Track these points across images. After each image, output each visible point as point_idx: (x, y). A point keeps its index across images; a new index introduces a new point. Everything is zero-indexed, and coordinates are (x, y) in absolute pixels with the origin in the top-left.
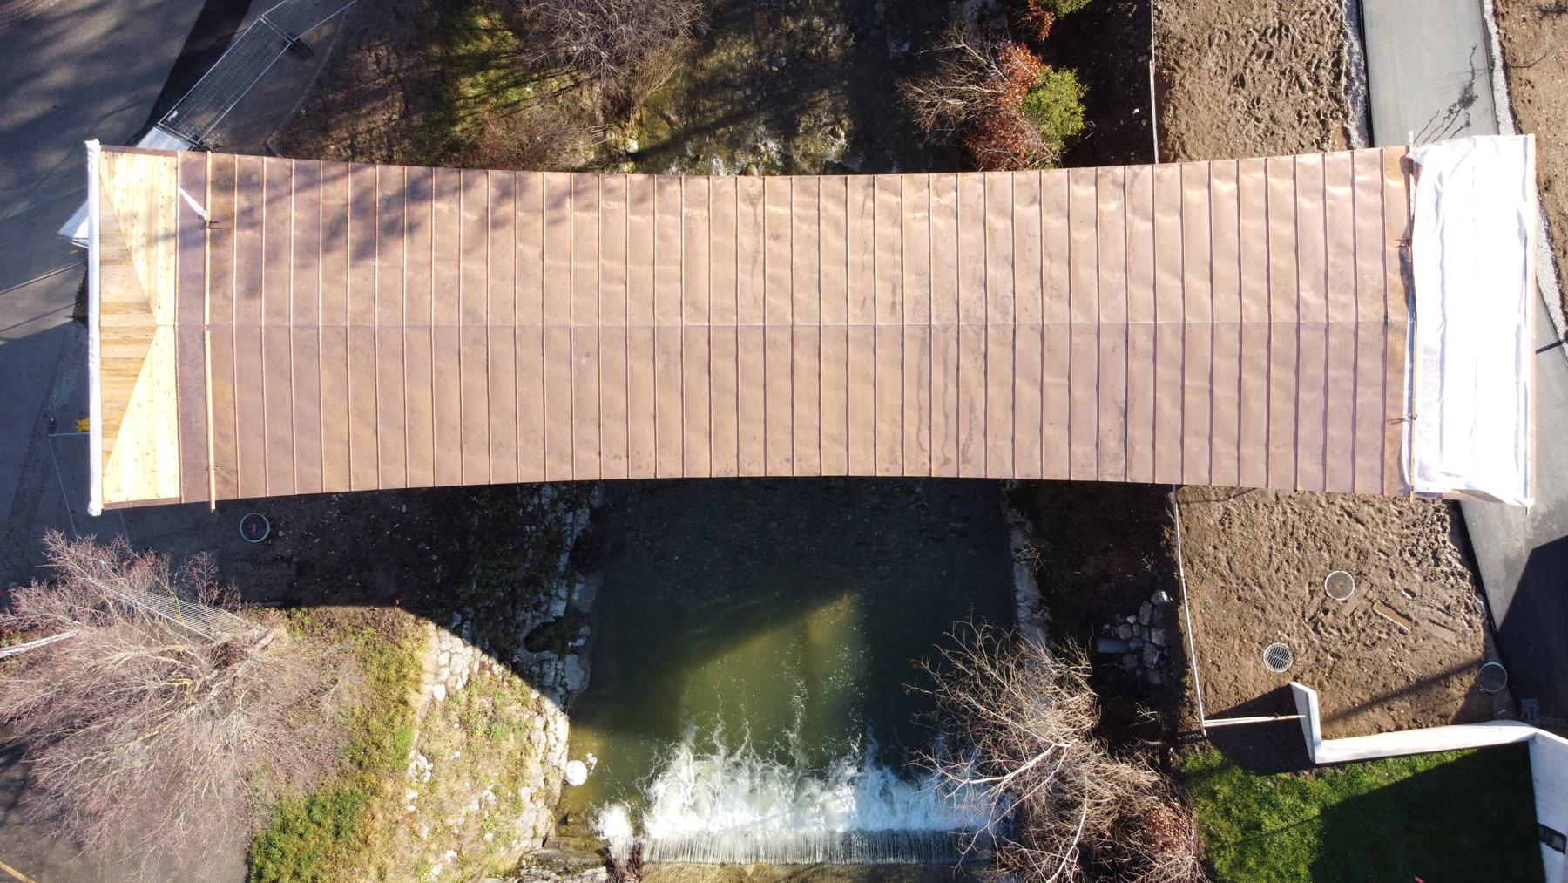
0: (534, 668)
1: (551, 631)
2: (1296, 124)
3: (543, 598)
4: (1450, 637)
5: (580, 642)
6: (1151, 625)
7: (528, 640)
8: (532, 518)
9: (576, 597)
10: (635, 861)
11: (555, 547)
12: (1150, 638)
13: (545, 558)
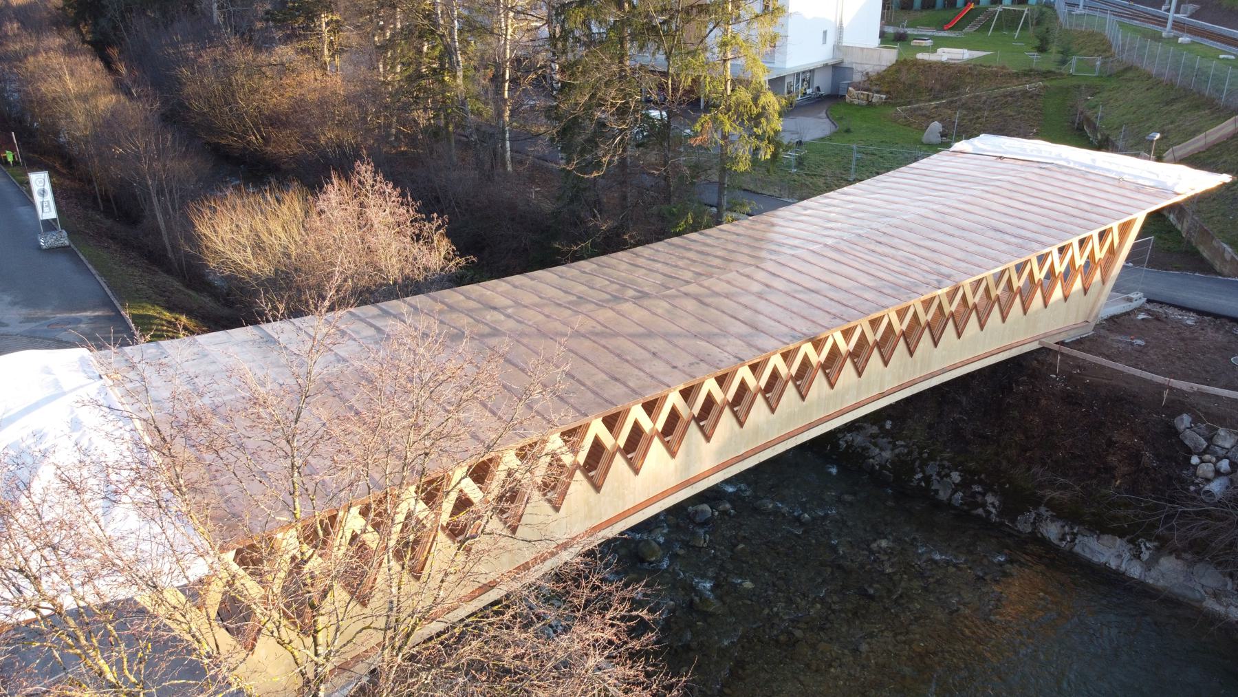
12: (1223, 448)
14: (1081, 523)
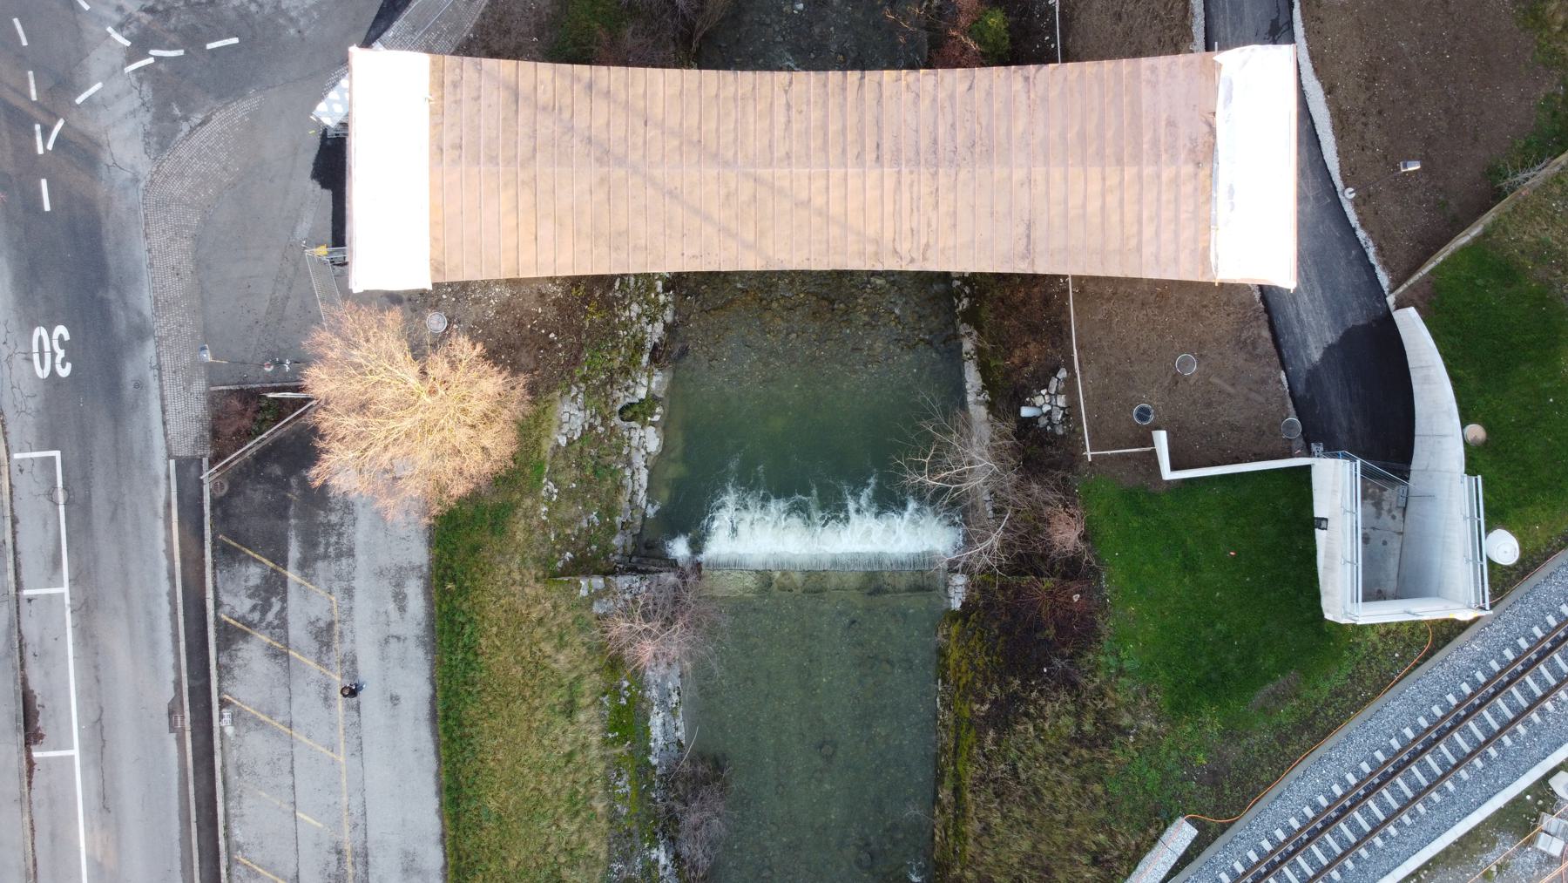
0: (625, 433)
1: (636, 408)
2: (1157, 46)
3: (631, 384)
4: (1261, 399)
5: (657, 418)
6: (1057, 393)
7: (621, 412)
8: (625, 326)
9: (653, 386)
10: (698, 567)
11: (639, 347)
13: (633, 355)
14: (979, 357)
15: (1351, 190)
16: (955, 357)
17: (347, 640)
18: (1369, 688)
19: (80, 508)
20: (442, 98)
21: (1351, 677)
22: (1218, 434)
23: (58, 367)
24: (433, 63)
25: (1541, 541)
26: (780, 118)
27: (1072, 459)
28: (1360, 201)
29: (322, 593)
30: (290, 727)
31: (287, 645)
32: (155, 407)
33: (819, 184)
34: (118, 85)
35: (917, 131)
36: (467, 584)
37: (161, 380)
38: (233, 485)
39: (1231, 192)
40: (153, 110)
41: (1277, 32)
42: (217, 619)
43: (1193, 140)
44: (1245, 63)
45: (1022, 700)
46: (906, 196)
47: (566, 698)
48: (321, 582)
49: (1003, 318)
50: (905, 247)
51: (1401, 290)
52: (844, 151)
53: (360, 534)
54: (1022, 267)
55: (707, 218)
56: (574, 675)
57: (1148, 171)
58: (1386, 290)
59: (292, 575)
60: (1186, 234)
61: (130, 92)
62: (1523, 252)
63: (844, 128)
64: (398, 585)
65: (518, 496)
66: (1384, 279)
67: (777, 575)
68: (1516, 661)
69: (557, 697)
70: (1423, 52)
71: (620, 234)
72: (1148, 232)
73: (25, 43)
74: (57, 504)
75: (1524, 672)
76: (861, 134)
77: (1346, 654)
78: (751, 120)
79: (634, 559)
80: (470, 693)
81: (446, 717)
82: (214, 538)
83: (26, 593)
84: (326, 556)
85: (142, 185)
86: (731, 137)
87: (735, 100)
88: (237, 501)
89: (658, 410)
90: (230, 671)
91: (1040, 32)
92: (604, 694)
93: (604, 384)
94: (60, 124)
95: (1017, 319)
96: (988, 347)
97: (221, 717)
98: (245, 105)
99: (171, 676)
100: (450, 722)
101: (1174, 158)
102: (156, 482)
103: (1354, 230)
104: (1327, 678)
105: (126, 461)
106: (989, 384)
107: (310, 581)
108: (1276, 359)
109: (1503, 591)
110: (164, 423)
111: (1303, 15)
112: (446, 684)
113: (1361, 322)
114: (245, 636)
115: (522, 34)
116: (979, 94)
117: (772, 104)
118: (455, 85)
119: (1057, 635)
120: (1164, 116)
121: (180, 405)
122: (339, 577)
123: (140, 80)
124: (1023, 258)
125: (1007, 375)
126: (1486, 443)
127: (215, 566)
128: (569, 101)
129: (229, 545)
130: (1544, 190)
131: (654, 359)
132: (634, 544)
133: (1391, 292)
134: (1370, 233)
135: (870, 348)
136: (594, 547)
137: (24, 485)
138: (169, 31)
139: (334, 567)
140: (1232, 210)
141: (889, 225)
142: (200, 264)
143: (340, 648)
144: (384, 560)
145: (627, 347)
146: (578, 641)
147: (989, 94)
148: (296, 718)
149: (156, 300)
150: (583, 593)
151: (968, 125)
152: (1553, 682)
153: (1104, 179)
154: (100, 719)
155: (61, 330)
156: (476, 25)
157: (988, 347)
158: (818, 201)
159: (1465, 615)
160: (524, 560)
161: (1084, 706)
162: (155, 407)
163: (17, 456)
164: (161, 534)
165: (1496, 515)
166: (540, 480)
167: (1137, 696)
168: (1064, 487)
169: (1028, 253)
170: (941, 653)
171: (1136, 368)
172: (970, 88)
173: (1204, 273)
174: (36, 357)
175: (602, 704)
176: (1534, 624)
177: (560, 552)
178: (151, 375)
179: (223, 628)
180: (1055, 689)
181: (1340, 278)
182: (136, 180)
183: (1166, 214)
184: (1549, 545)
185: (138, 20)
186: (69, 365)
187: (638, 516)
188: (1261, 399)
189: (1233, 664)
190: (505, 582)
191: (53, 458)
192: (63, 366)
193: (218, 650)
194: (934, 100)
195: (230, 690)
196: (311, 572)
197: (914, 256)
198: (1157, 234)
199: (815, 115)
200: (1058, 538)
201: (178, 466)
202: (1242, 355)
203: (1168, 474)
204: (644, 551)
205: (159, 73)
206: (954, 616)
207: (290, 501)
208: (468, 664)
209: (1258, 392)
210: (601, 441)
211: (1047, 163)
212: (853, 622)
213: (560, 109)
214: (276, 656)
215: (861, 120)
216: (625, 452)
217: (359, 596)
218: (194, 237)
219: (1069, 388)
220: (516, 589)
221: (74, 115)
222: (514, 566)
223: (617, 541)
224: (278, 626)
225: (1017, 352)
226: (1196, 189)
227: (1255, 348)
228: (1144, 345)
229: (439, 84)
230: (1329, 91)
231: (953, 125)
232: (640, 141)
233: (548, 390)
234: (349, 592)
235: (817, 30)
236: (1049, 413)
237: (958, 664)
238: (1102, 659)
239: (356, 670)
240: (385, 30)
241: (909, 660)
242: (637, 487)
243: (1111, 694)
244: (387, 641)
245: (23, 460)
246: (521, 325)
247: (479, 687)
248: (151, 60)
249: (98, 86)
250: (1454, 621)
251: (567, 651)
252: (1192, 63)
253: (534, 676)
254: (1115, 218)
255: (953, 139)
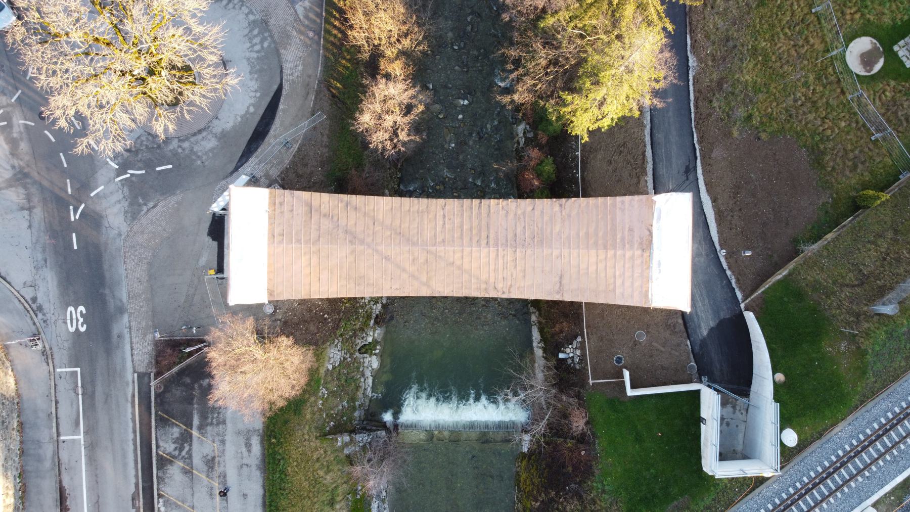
1: (367, 347)
4: (677, 354)
5: (377, 351)
6: (576, 348)
8: (362, 307)
9: (376, 335)
10: (396, 426)
11: (369, 317)
15: (724, 251)
16: (528, 324)
17: (222, 466)
18: (723, 506)
19: (89, 397)
20: (275, 210)
21: (714, 500)
22: (656, 371)
23: (80, 327)
24: (271, 193)
25: (808, 435)
26: (440, 222)
27: (583, 383)
28: (728, 256)
29: (210, 442)
30: (193, 508)
31: (192, 468)
32: (128, 347)
33: (458, 255)
34: (112, 187)
35: (507, 230)
36: (282, 440)
37: (130, 334)
38: (165, 387)
39: (659, 264)
40: (129, 200)
41: (686, 182)
42: (157, 454)
43: (641, 238)
44: (667, 201)
45: (555, 501)
46: (501, 261)
47: (330, 497)
48: (209, 436)
49: (551, 308)
50: (500, 286)
51: (747, 301)
52: (471, 239)
53: (229, 415)
54: (557, 297)
55: (404, 270)
56: (334, 485)
57: (619, 253)
58: (740, 301)
59: (195, 433)
60: (637, 284)
61: (117, 191)
62: (807, 285)
63: (471, 227)
64: (247, 439)
65: (308, 396)
66: (739, 295)
67: (436, 432)
68: (795, 494)
69: (326, 497)
70: (762, 179)
71: (360, 278)
72: (619, 282)
73: (65, 166)
74: (78, 395)
75: (798, 499)
76: (479, 231)
77: (712, 488)
78: (426, 223)
79: (365, 423)
80: (282, 494)
81: (271, 505)
82: (156, 413)
83: (62, 438)
84: (212, 424)
85: (123, 237)
86: (415, 231)
87: (418, 213)
88: (168, 395)
89: (378, 347)
90: (163, 480)
91: (571, 168)
92: (349, 494)
93: (351, 337)
94: (83, 206)
95: (557, 309)
96: (544, 321)
97: (159, 502)
98: (175, 198)
99: (133, 481)
100: (272, 508)
101: (632, 247)
102: (127, 384)
103: (725, 271)
104: (703, 500)
105: (113, 374)
106: (544, 339)
107: (203, 436)
108: (685, 334)
109: (789, 460)
110: (132, 355)
111: (702, 163)
112: (271, 489)
113: (728, 317)
114: (171, 462)
115: (314, 166)
116: (537, 213)
117: (436, 215)
118: (281, 204)
119: (573, 471)
120: (627, 226)
121: (140, 347)
122: (218, 434)
123: (123, 185)
124: (558, 293)
125: (553, 336)
126: (785, 383)
127: (156, 428)
128: (337, 212)
129: (164, 417)
130: (819, 254)
131: (376, 323)
132: (365, 414)
133: (743, 302)
134: (733, 272)
135: (485, 317)
136: (345, 418)
137: (63, 386)
138: (138, 161)
139: (216, 429)
140: (660, 272)
141: (492, 275)
142: (151, 277)
143: (218, 470)
144: (240, 426)
145: (363, 317)
146: (336, 469)
147: (542, 212)
148: (196, 504)
149: (129, 295)
150: (339, 444)
151: (532, 227)
152: (813, 504)
153: (597, 256)
154: (98, 502)
155: (82, 308)
156: (291, 161)
157: (544, 321)
158: (458, 263)
159: (767, 474)
160: (310, 428)
161: (586, 507)
162: (128, 347)
163: (58, 370)
164: (130, 410)
165: (785, 421)
166: (318, 388)
167: (611, 504)
168: (578, 396)
169: (560, 291)
170: (518, 474)
171: (615, 337)
172: (533, 209)
173: (645, 303)
174: (69, 321)
175: (348, 498)
176: (804, 476)
177: (328, 423)
178: (126, 331)
179: (161, 459)
180: (572, 498)
181: (718, 295)
182: (120, 235)
183: (628, 274)
184: (812, 437)
185: (122, 155)
186: (85, 326)
187: (367, 401)
188: (677, 354)
189: (657, 491)
190: (301, 440)
191: (76, 372)
192: (82, 326)
193: (158, 469)
194: (516, 215)
195: (163, 489)
196: (204, 431)
197: (505, 290)
198: (623, 283)
199: (457, 221)
200: (575, 425)
201: (138, 377)
202: (668, 332)
203: (630, 392)
204: (370, 418)
205: (132, 182)
206: (524, 455)
207: (194, 395)
208: (282, 479)
209: (676, 350)
210: (349, 366)
211: (570, 248)
212: (474, 457)
213: (332, 216)
214: (186, 473)
215: (479, 224)
216: (361, 370)
217: (228, 444)
218: (148, 263)
219: (582, 347)
220: (306, 443)
221: (90, 202)
222: (305, 432)
223: (356, 414)
224: (187, 458)
225: (558, 326)
226: (642, 262)
227: (675, 328)
228: (620, 326)
229: (273, 203)
230: (714, 201)
231: (524, 227)
232: (371, 232)
233: (324, 343)
234: (223, 442)
235: (461, 157)
236: (573, 357)
237: (525, 481)
238: (595, 484)
239: (226, 481)
240: (245, 162)
241: (501, 476)
242: (367, 386)
243: (598, 502)
244: (241, 467)
245: (61, 372)
246: (311, 311)
247: (287, 491)
248: (128, 176)
249: (102, 188)
250: (763, 477)
251: (331, 474)
252: (641, 200)
253: (314, 487)
254: (603, 275)
255: (525, 234)
